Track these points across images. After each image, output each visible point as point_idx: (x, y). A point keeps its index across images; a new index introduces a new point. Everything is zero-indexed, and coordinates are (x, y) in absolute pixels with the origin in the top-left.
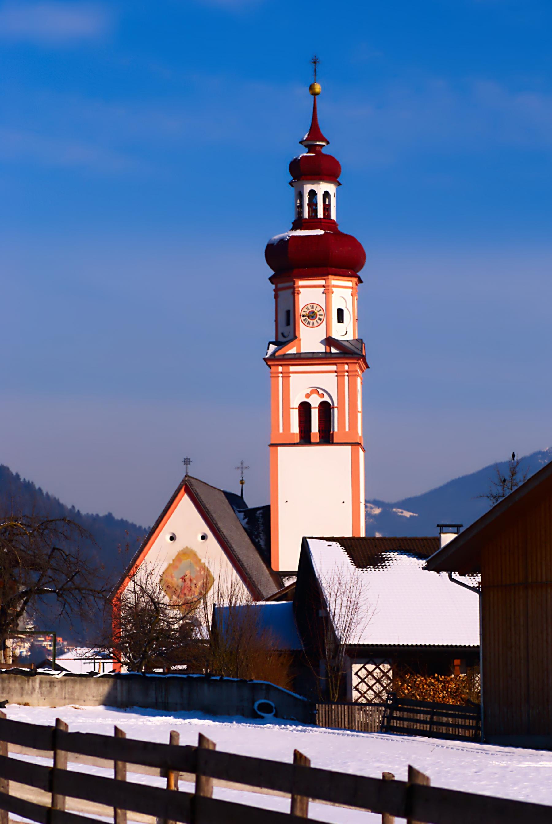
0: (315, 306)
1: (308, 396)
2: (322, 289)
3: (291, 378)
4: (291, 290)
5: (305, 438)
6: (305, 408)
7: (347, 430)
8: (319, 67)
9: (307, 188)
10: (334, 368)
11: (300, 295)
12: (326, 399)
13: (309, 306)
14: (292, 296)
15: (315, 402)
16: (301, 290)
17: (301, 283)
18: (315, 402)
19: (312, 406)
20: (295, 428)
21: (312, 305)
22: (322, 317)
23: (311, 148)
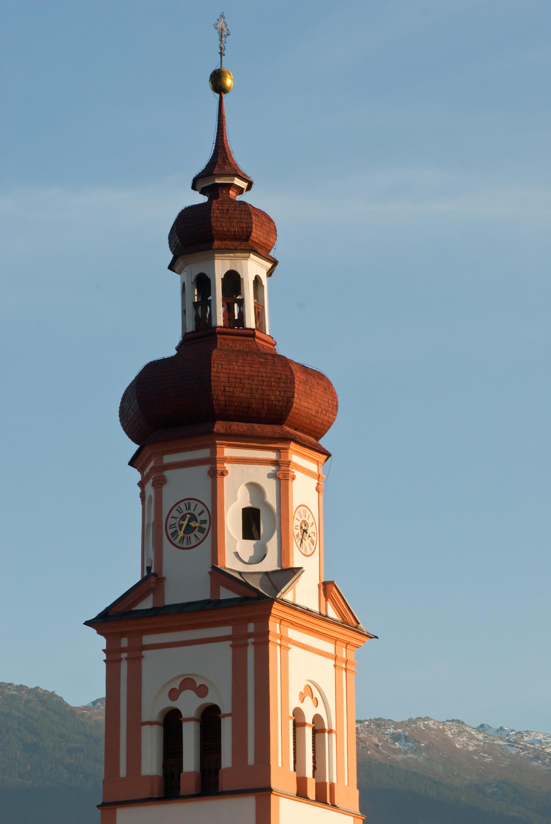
0: (193, 503)
1: (174, 694)
2: (271, 469)
3: (290, 652)
4: (207, 468)
5: (169, 788)
6: (172, 722)
7: (280, 765)
8: (229, 42)
9: (221, 267)
10: (227, 630)
11: (226, 478)
12: (210, 699)
13: (182, 505)
14: (209, 481)
15: (189, 705)
16: (228, 466)
17: (228, 452)
18: (189, 705)
19: (185, 715)
20: (151, 764)
21: (186, 502)
22: (206, 526)
23: (213, 191)
